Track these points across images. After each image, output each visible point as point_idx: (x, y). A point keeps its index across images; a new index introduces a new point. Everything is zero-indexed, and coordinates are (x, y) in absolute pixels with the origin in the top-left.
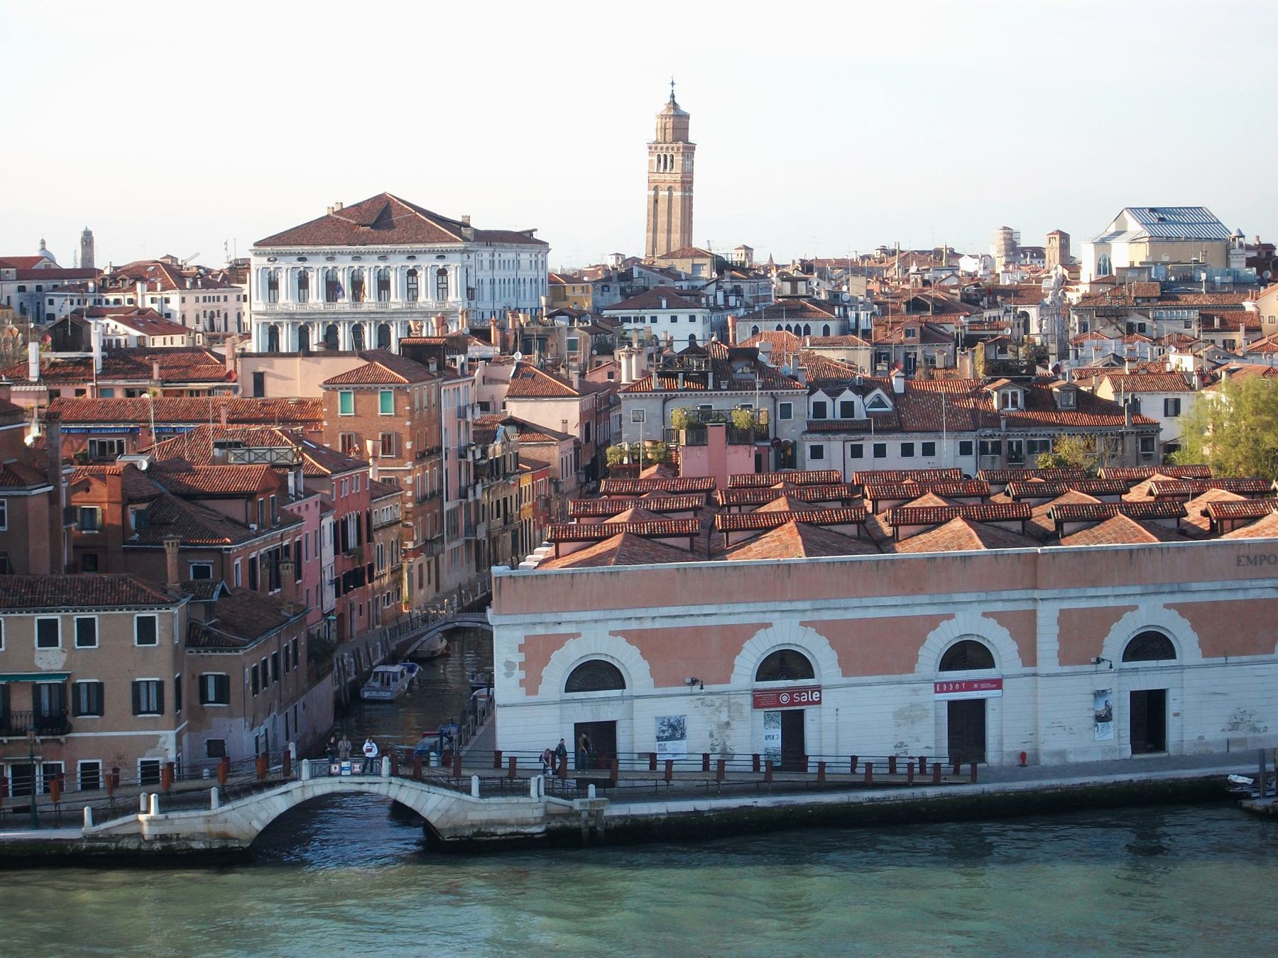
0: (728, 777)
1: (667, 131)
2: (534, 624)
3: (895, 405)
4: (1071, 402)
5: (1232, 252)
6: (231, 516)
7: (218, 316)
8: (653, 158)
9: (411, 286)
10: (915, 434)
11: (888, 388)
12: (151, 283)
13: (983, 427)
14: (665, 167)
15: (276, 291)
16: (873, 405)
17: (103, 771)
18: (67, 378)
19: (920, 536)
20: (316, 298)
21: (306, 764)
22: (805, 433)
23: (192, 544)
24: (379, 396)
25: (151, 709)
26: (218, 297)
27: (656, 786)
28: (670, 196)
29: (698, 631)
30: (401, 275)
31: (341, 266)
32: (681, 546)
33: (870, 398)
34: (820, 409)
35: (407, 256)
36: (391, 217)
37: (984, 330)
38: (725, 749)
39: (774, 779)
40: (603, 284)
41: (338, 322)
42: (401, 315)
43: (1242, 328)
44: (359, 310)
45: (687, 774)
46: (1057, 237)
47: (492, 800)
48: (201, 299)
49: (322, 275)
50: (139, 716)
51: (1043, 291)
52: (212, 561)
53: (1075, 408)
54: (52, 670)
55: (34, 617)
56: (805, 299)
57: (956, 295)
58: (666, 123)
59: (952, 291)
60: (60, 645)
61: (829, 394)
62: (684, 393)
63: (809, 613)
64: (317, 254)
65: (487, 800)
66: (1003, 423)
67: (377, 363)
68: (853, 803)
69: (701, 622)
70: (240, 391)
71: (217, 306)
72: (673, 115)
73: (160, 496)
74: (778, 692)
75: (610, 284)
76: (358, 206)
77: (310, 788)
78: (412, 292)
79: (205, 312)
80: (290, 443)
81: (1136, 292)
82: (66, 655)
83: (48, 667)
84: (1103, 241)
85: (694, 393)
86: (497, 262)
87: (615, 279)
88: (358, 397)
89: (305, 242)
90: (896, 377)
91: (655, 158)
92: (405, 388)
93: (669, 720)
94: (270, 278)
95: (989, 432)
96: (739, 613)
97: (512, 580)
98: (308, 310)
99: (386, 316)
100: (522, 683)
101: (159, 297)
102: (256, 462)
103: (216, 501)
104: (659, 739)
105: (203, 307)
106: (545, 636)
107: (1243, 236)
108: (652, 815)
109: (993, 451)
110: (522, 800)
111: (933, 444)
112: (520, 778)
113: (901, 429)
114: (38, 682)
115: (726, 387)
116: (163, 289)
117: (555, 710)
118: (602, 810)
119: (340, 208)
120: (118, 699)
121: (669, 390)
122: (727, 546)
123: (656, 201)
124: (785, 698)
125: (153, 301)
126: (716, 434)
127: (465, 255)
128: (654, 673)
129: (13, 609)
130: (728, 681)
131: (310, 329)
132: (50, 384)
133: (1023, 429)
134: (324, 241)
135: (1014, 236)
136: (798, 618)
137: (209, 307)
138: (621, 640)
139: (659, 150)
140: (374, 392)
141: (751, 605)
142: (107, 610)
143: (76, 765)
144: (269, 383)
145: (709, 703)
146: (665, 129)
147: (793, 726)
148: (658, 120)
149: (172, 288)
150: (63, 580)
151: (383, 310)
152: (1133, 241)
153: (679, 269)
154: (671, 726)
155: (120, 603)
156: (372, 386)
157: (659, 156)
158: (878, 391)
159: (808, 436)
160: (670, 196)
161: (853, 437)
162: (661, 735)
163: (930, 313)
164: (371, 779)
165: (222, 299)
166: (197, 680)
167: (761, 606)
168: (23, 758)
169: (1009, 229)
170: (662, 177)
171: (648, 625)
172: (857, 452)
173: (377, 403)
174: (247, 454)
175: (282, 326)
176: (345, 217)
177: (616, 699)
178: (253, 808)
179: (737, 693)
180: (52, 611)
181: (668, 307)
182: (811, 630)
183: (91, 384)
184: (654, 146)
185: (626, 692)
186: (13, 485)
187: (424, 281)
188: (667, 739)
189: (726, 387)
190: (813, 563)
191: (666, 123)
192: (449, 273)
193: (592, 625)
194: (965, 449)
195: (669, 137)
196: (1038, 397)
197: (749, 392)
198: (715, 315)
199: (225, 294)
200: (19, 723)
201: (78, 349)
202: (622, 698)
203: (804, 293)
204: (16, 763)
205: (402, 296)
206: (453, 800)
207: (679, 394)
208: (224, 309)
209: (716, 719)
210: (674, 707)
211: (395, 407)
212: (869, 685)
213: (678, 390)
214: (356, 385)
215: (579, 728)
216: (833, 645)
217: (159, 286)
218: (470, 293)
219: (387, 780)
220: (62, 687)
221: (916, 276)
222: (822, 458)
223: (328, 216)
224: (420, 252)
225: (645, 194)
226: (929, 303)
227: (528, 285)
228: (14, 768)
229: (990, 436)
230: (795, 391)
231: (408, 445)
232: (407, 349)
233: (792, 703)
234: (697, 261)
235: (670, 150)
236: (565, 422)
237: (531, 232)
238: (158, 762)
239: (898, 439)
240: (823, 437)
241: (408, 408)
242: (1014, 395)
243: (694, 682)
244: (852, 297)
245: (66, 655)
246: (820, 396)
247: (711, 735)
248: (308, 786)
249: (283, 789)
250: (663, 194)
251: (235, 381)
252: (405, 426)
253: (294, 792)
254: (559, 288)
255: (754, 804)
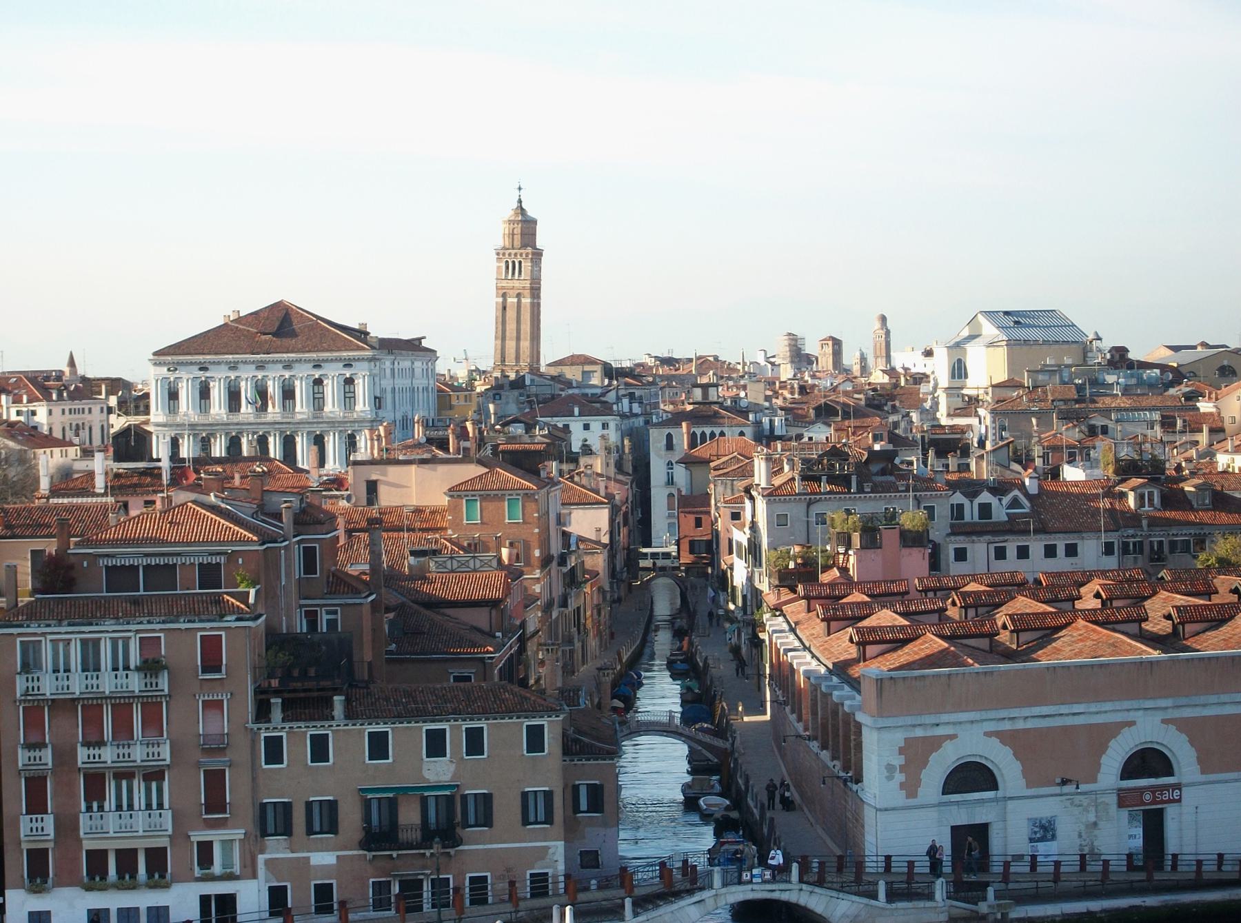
0: (1112, 877)
1: (515, 236)
2: (914, 726)
3: (1032, 506)
4: (1207, 501)
5: (1090, 355)
6: (475, 624)
7: (83, 429)
8: (501, 264)
9: (316, 396)
10: (1058, 535)
11: (1022, 487)
12: (15, 395)
13: (1125, 527)
14: (513, 273)
15: (176, 402)
16: (1011, 506)
17: (492, 885)
18: (134, 489)
19: (1207, 633)
20: (218, 408)
21: (718, 872)
22: (949, 535)
23: (453, 653)
24: (506, 503)
25: (539, 820)
26: (83, 409)
27: (1037, 888)
28: (519, 302)
29: (1066, 730)
30: (306, 384)
31: (244, 376)
32: (981, 647)
33: (1006, 500)
34: (958, 510)
35: (312, 364)
36: (292, 325)
37: (946, 434)
38: (1093, 849)
39: (1156, 878)
40: (494, 392)
41: (241, 433)
42: (307, 426)
43: (1205, 429)
44: (263, 420)
45: (1066, 875)
46: (830, 343)
47: (900, 905)
48: (67, 412)
49: (224, 385)
50: (528, 827)
51: (921, 396)
52: (474, 671)
53: (1211, 507)
54: (440, 782)
55: (421, 728)
56: (717, 405)
57: (860, 399)
58: (514, 229)
59: (856, 396)
60: (448, 755)
61: (965, 495)
62: (828, 496)
63: (1170, 710)
64: (219, 363)
65: (894, 905)
66: (1145, 523)
67: (498, 469)
68: (1234, 901)
69: (1069, 721)
70: (353, 500)
71: (83, 419)
72: (521, 221)
73: (403, 605)
74: (1141, 790)
75: (502, 393)
76: (256, 313)
77: (723, 897)
78: (318, 401)
79: (71, 424)
80: (457, 549)
81: (1052, 395)
82: (454, 765)
83: (436, 779)
84: (958, 345)
85: (838, 496)
86: (396, 371)
87: (507, 387)
88: (484, 504)
89: (206, 351)
90: (1031, 478)
91: (503, 265)
92: (534, 494)
93: (1040, 822)
94: (170, 388)
95: (1131, 532)
96: (1106, 712)
97: (892, 681)
98: (211, 420)
99: (291, 426)
100: (902, 786)
101: (25, 409)
102: (481, 569)
103: (457, 609)
104: (1031, 840)
105: (69, 419)
106: (925, 738)
107: (1099, 339)
108: (1048, 917)
109: (1135, 552)
110: (929, 904)
111: (1076, 544)
112: (918, 883)
113: (1042, 530)
114: (426, 794)
115: (869, 490)
116: (29, 401)
117: (933, 814)
118: (1007, 913)
119: (237, 317)
120: (507, 810)
121: (812, 493)
122: (1018, 646)
123: (504, 308)
124: (1148, 797)
125: (19, 413)
126: (889, 537)
127: (373, 363)
128: (1025, 773)
129: (401, 720)
130: (1094, 780)
131: (212, 440)
132: (117, 495)
133: (1163, 528)
134: (225, 351)
135: (799, 342)
136: (1160, 716)
137: (75, 420)
138: (995, 741)
139: (507, 256)
140: (501, 499)
141: (1117, 703)
142: (496, 719)
143: (465, 879)
144: (382, 490)
145: (1077, 802)
146: (513, 234)
147: (1154, 825)
148: (505, 225)
149: (38, 400)
150: (441, 688)
151: (288, 420)
152: (991, 345)
153: (569, 376)
154: (1042, 827)
155: (509, 712)
156: (500, 493)
157: (507, 262)
158: (1016, 492)
159: (953, 538)
160: (519, 302)
161: (997, 539)
162: (1034, 836)
163: (839, 418)
164: (782, 886)
165: (87, 411)
166: (569, 790)
167: (1127, 704)
168: (409, 873)
169: (794, 335)
170: (510, 284)
171: (1020, 725)
172: (1001, 554)
173: (504, 511)
174: (472, 561)
175: (183, 438)
176: (244, 325)
177: (991, 800)
178: (667, 918)
179: (1104, 792)
180: (441, 721)
181: (580, 415)
182: (1172, 728)
183: (161, 495)
184: (501, 252)
185: (1000, 793)
186: (348, 593)
187: (331, 390)
188: (1040, 840)
189: (869, 490)
190: (1173, 660)
191: (514, 229)
192: (356, 382)
193: (969, 726)
194: (1108, 549)
195: (517, 243)
196: (1175, 499)
197: (893, 494)
198: (626, 421)
199: (90, 406)
200: (405, 837)
201: (142, 460)
202: (996, 800)
203: (715, 399)
204: (403, 878)
205: (308, 406)
206: (862, 906)
207: (823, 497)
208: (88, 421)
209: (1084, 821)
210: (1046, 808)
211: (523, 514)
212: (1226, 782)
213: (820, 493)
214: (483, 493)
215: (955, 829)
216: (1192, 742)
217: (25, 398)
218: (378, 402)
219: (798, 887)
220: (450, 800)
221: (793, 382)
222: (965, 560)
223: (226, 325)
224: (326, 361)
225: (494, 300)
226: (838, 408)
227: (421, 394)
228: (400, 882)
229: (1133, 536)
230: (934, 493)
231: (537, 553)
232: (506, 456)
233: (1154, 802)
234: (587, 368)
235: (519, 256)
236: (599, 530)
237: (420, 340)
238: (546, 874)
239: (1041, 540)
240: (967, 539)
241: (536, 515)
242: (1151, 494)
243: (1064, 782)
244: (750, 403)
245: (454, 765)
246: (958, 498)
247: (1080, 836)
248: (721, 895)
249: (696, 898)
250: (512, 300)
251: (347, 490)
252: (533, 533)
253: (707, 900)
254: (445, 396)
255: (1143, 904)
